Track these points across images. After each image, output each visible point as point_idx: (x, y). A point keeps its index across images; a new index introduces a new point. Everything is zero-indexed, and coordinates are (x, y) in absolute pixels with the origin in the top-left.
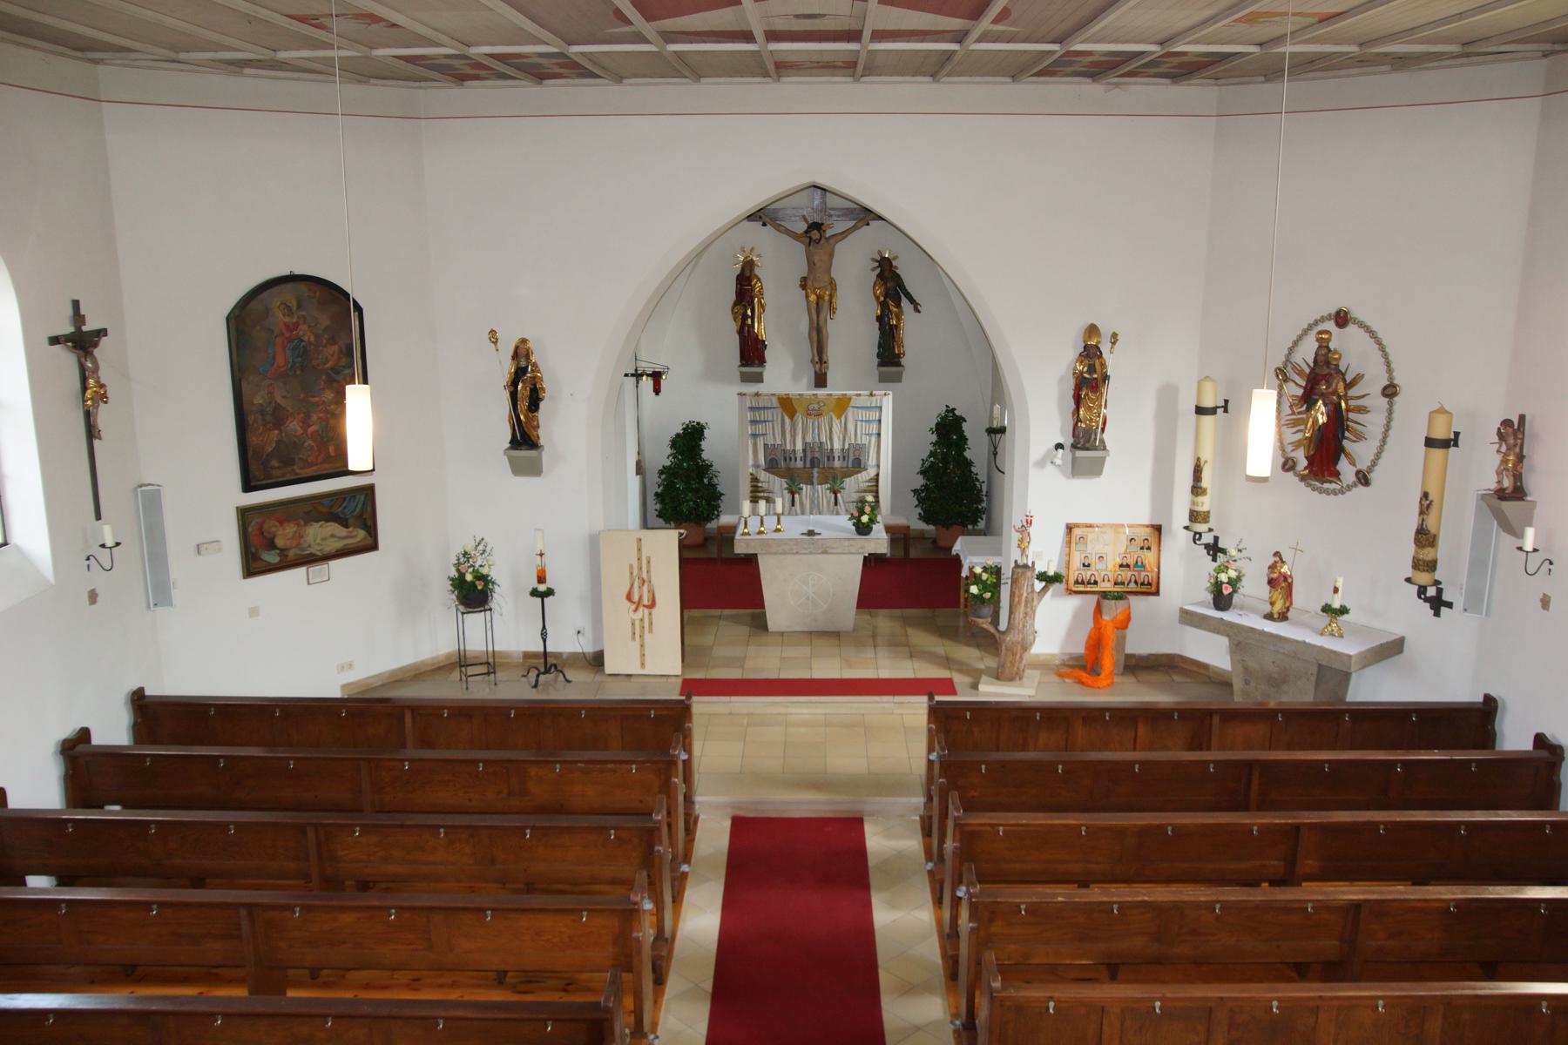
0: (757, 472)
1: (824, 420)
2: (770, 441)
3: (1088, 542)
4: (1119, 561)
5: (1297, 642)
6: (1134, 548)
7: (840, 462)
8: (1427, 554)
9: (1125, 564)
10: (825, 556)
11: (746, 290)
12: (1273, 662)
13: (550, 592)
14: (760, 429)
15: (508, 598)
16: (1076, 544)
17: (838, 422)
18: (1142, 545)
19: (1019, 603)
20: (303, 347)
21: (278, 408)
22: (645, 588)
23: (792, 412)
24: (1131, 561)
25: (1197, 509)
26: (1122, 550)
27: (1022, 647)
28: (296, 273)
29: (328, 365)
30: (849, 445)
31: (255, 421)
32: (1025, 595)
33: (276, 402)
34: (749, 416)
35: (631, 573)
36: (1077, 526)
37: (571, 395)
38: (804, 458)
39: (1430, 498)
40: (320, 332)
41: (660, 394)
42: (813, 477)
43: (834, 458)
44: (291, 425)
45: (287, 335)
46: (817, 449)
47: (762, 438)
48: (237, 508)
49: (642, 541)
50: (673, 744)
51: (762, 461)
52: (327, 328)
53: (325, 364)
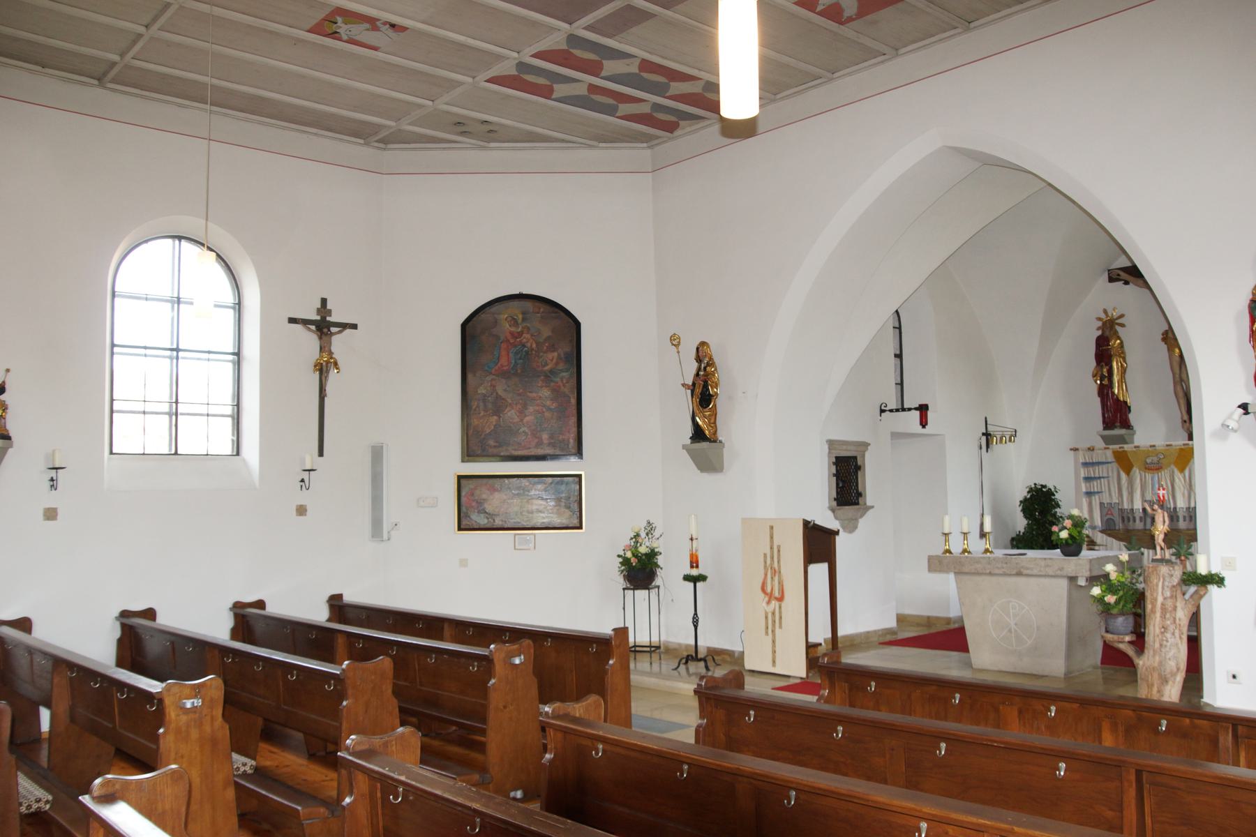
0: (1093, 534)
1: (1164, 475)
2: (1106, 500)
7: (1186, 522)
10: (1021, 581)
13: (702, 578)
14: (1095, 486)
15: (671, 569)
17: (1181, 476)
19: (1153, 611)
20: (526, 351)
21: (498, 397)
22: (776, 579)
23: (1127, 468)
27: (1160, 675)
28: (524, 293)
29: (547, 368)
31: (478, 406)
32: (1160, 599)
33: (497, 393)
34: (1083, 472)
35: (765, 562)
37: (744, 393)
40: (541, 341)
43: (1178, 517)
44: (509, 414)
48: (463, 461)
49: (774, 528)
50: (701, 729)
52: (548, 338)
53: (544, 366)
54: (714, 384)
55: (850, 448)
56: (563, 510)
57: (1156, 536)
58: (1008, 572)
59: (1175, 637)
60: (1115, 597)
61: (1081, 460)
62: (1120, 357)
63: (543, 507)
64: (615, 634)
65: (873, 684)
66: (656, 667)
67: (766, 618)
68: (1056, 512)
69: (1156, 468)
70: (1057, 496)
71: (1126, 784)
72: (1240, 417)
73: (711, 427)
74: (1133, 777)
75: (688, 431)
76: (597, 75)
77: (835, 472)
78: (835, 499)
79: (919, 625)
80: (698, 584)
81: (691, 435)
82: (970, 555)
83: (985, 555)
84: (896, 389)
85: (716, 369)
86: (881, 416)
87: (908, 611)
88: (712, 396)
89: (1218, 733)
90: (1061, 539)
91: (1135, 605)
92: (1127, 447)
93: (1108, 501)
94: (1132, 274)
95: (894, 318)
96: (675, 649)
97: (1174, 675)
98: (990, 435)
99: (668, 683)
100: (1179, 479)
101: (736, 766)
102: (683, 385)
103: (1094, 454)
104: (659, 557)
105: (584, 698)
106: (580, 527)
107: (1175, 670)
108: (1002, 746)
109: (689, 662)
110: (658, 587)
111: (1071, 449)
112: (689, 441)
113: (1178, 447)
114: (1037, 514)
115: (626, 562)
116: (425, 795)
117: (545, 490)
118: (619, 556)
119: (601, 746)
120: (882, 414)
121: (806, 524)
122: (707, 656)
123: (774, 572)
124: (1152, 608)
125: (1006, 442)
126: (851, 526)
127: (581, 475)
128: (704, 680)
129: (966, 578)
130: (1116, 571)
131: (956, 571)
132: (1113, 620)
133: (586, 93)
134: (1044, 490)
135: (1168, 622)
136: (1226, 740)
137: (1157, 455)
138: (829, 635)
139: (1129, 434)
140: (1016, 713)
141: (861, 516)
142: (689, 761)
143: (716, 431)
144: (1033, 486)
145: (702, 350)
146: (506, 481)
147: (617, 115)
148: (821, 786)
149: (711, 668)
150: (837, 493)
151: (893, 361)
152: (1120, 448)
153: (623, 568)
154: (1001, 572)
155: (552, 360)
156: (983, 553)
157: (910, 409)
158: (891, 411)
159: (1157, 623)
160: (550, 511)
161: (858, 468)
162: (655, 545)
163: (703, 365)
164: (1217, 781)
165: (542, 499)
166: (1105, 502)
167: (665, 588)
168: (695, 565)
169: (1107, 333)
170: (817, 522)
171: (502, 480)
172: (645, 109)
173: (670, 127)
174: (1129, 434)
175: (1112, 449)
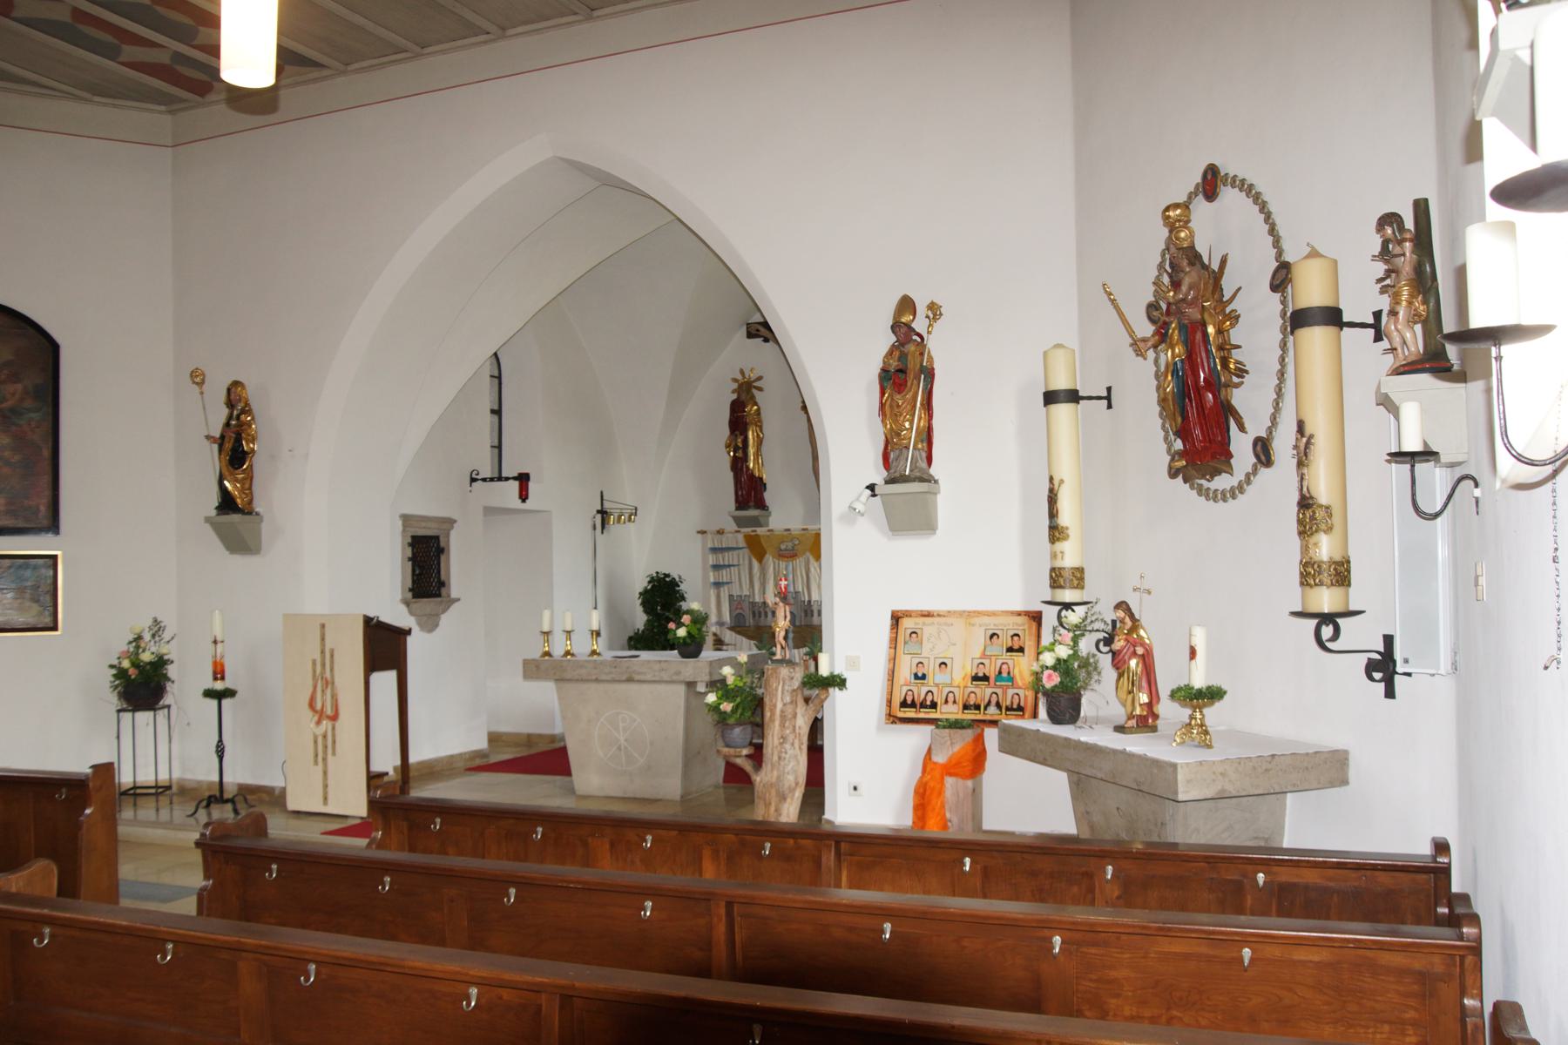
0: (721, 632)
1: (799, 563)
2: (736, 592)
4: (970, 670)
5: (1115, 751)
6: (998, 648)
8: (1325, 548)
9: (981, 674)
12: (1118, 809)
13: (229, 693)
14: (724, 575)
16: (905, 643)
18: (1010, 644)
19: (772, 720)
25: (1058, 564)
27: (778, 792)
32: (779, 706)
34: (711, 559)
35: (314, 671)
36: (908, 614)
37: (290, 451)
39: (1308, 431)
43: (812, 611)
49: (326, 625)
50: (205, 893)
51: (727, 618)
55: (429, 524)
56: (28, 604)
57: (777, 634)
60: (731, 705)
61: (710, 545)
65: (438, 820)
67: (316, 742)
68: (681, 606)
70: (683, 587)
71: (715, 919)
72: (868, 498)
74: (723, 911)
75: (214, 499)
77: (410, 556)
78: (410, 590)
79: (517, 745)
80: (226, 702)
81: (217, 504)
82: (574, 658)
83: (590, 658)
84: (492, 452)
85: (253, 419)
86: (471, 486)
89: (821, 851)
90: (679, 638)
91: (752, 709)
92: (761, 531)
93: (739, 594)
94: (761, 331)
95: (491, 364)
97: (792, 790)
98: (606, 512)
100: (815, 568)
102: (208, 437)
103: (724, 538)
105: (26, 865)
106: (55, 628)
107: (794, 785)
110: (169, 707)
111: (699, 532)
112: (214, 513)
113: (814, 532)
115: (121, 674)
118: (112, 666)
119: (47, 931)
120: (474, 484)
121: (368, 621)
125: (625, 522)
126: (430, 624)
127: (55, 557)
128: (210, 828)
129: (568, 686)
130: (733, 675)
132: (729, 732)
134: (667, 579)
135: (788, 732)
136: (829, 858)
137: (792, 540)
138: (398, 762)
140: (607, 846)
141: (444, 612)
144: (655, 575)
145: (235, 393)
147: (121, 59)
148: (345, 954)
151: (488, 420)
152: (753, 531)
153: (117, 682)
154: (609, 678)
155: (14, 394)
156: (589, 656)
157: (507, 479)
158: (484, 480)
159: (776, 732)
160: (8, 606)
161: (441, 551)
162: (164, 650)
163: (235, 413)
164: (806, 906)
168: (219, 676)
169: (743, 397)
172: (164, 58)
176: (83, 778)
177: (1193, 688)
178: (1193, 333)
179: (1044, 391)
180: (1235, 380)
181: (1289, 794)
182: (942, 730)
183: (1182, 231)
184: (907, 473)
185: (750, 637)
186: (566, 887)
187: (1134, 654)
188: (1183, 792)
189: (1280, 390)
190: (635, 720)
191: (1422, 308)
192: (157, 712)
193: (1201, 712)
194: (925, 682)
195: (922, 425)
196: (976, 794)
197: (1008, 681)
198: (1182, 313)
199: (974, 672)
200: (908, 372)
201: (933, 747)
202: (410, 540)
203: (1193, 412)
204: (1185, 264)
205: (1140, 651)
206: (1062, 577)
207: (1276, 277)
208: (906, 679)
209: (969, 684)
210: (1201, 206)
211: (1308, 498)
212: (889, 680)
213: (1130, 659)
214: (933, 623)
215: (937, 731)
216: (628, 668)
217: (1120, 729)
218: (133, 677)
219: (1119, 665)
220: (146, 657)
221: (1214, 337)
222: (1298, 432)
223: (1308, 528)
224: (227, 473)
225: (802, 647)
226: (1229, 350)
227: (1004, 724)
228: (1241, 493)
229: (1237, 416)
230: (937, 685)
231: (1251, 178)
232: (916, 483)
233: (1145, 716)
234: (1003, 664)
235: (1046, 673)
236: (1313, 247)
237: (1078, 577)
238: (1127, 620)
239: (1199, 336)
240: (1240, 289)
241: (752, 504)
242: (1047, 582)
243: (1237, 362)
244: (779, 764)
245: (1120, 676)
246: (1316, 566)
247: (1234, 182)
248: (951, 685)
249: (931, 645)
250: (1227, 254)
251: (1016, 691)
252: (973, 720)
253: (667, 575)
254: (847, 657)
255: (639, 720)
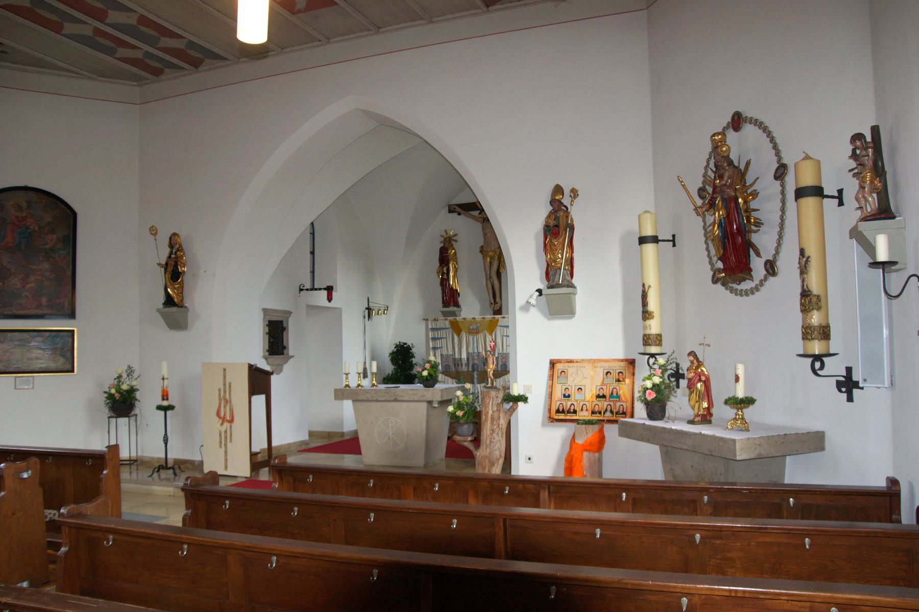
1: (480, 336)
2: (445, 353)
3: (569, 374)
4: (595, 392)
6: (610, 380)
8: (815, 319)
9: (601, 394)
11: (445, 258)
12: (692, 466)
13: (171, 407)
15: (147, 402)
16: (558, 377)
18: (617, 377)
19: (486, 420)
24: (607, 392)
25: (648, 332)
26: (599, 383)
27: (490, 461)
30: (498, 354)
32: (490, 412)
35: (220, 395)
36: (559, 361)
38: (467, 365)
39: (807, 254)
41: (331, 301)
42: (474, 377)
45: (17, 223)
46: (476, 358)
47: (439, 350)
49: (227, 370)
50: (187, 517)
54: (182, 265)
57: (488, 372)
58: (388, 399)
59: (499, 436)
60: (463, 412)
61: (430, 327)
62: (454, 261)
63: (40, 355)
64: (108, 451)
65: (311, 476)
66: (134, 475)
67: (220, 435)
68: (412, 361)
69: (476, 332)
70: (413, 350)
72: (537, 297)
73: (179, 296)
74: (502, 524)
75: (162, 299)
76: (102, 22)
78: (268, 351)
80: (169, 413)
81: (163, 302)
82: (363, 388)
83: (372, 388)
85: (184, 254)
86: (300, 293)
87: (314, 429)
88: (180, 273)
90: (423, 376)
96: (149, 462)
97: (498, 460)
98: (370, 309)
99: (146, 487)
101: (230, 542)
102: (159, 264)
103: (438, 323)
104: (138, 392)
106: (73, 371)
107: (499, 457)
108: (415, 511)
109: (161, 470)
112: (161, 306)
113: (489, 319)
114: (400, 362)
115: (110, 397)
116: (594, 486)
117: (43, 342)
118: (105, 392)
119: (111, 537)
120: (301, 292)
121: (251, 367)
122: (174, 465)
123: (227, 402)
124: (485, 418)
125: (381, 314)
127: (73, 331)
128: (189, 480)
131: (354, 399)
133: (91, 34)
134: (405, 346)
135: (495, 427)
136: (544, 495)
139: (458, 311)
140: (412, 490)
141: (285, 363)
142: (189, 541)
143: (183, 299)
144: (398, 343)
146: (9, 334)
149: (178, 474)
150: (269, 346)
151: (309, 256)
153: (108, 401)
155: (51, 241)
156: (371, 387)
158: (307, 290)
162: (134, 383)
163: (174, 251)
165: (41, 349)
166: (444, 353)
167: (141, 416)
169: (447, 245)
170: (258, 366)
171: (5, 334)
172: (138, 54)
173: (157, 72)
174: (458, 311)
175: (449, 320)
176: (102, 453)
177: (738, 398)
178: (731, 203)
179: (639, 236)
180: (753, 228)
181: (788, 457)
182: (581, 426)
183: (724, 147)
184: (560, 283)
185: (452, 378)
186: (407, 512)
187: (700, 380)
188: (739, 455)
189: (781, 234)
190: (398, 423)
191: (879, 185)
192: (130, 418)
193: (742, 412)
194: (570, 399)
195: (568, 256)
196: (600, 460)
197: (616, 398)
198: (724, 192)
199: (598, 393)
200: (560, 226)
201: (576, 435)
202: (267, 323)
203: (730, 247)
204: (725, 165)
205: (703, 378)
206: (650, 339)
207: (778, 172)
208: (559, 397)
209: (595, 400)
210: (731, 135)
211: (807, 291)
212: (549, 398)
213: (697, 383)
214: (574, 366)
215: (578, 426)
216: (394, 393)
217: (691, 422)
218: (117, 398)
219: (691, 386)
220: (125, 387)
221: (742, 206)
222: (800, 254)
223: (807, 307)
224: (169, 284)
225: (482, 383)
226: (750, 212)
227: (622, 421)
228: (758, 291)
229: (755, 248)
230: (577, 401)
231: (761, 118)
232: (565, 288)
233: (705, 415)
234: (614, 388)
235: (648, 392)
236: (806, 154)
237: (658, 340)
238: (695, 361)
239: (732, 205)
240: (758, 178)
241: (452, 304)
242: (642, 343)
243: (755, 218)
244: (491, 445)
245: (691, 393)
246: (812, 329)
247: (751, 121)
248: (584, 400)
249: (572, 379)
250: (750, 159)
251: (621, 403)
252: (598, 420)
253: (405, 344)
254: (524, 386)
255: (400, 423)
